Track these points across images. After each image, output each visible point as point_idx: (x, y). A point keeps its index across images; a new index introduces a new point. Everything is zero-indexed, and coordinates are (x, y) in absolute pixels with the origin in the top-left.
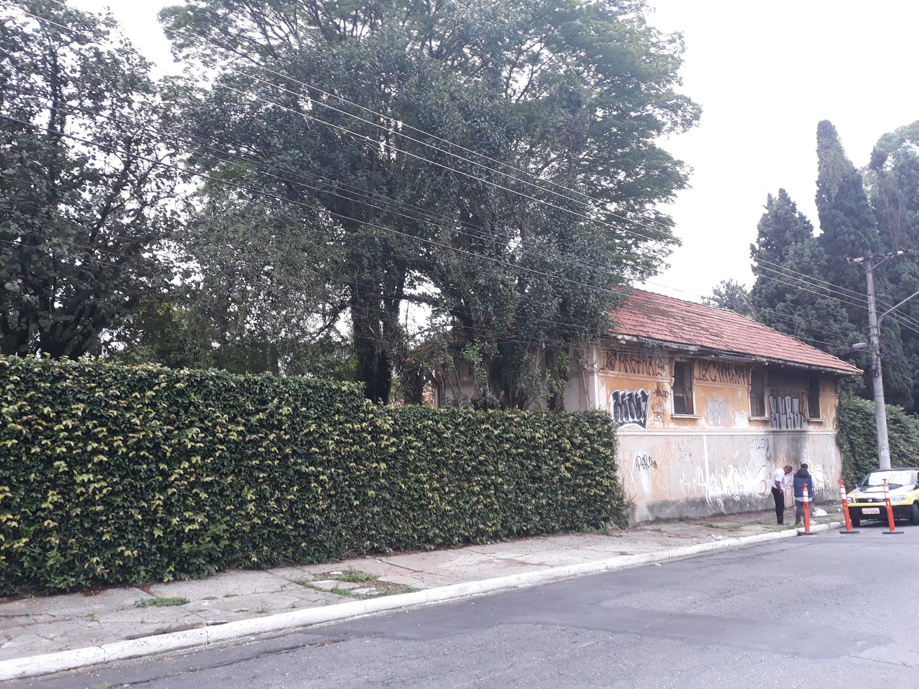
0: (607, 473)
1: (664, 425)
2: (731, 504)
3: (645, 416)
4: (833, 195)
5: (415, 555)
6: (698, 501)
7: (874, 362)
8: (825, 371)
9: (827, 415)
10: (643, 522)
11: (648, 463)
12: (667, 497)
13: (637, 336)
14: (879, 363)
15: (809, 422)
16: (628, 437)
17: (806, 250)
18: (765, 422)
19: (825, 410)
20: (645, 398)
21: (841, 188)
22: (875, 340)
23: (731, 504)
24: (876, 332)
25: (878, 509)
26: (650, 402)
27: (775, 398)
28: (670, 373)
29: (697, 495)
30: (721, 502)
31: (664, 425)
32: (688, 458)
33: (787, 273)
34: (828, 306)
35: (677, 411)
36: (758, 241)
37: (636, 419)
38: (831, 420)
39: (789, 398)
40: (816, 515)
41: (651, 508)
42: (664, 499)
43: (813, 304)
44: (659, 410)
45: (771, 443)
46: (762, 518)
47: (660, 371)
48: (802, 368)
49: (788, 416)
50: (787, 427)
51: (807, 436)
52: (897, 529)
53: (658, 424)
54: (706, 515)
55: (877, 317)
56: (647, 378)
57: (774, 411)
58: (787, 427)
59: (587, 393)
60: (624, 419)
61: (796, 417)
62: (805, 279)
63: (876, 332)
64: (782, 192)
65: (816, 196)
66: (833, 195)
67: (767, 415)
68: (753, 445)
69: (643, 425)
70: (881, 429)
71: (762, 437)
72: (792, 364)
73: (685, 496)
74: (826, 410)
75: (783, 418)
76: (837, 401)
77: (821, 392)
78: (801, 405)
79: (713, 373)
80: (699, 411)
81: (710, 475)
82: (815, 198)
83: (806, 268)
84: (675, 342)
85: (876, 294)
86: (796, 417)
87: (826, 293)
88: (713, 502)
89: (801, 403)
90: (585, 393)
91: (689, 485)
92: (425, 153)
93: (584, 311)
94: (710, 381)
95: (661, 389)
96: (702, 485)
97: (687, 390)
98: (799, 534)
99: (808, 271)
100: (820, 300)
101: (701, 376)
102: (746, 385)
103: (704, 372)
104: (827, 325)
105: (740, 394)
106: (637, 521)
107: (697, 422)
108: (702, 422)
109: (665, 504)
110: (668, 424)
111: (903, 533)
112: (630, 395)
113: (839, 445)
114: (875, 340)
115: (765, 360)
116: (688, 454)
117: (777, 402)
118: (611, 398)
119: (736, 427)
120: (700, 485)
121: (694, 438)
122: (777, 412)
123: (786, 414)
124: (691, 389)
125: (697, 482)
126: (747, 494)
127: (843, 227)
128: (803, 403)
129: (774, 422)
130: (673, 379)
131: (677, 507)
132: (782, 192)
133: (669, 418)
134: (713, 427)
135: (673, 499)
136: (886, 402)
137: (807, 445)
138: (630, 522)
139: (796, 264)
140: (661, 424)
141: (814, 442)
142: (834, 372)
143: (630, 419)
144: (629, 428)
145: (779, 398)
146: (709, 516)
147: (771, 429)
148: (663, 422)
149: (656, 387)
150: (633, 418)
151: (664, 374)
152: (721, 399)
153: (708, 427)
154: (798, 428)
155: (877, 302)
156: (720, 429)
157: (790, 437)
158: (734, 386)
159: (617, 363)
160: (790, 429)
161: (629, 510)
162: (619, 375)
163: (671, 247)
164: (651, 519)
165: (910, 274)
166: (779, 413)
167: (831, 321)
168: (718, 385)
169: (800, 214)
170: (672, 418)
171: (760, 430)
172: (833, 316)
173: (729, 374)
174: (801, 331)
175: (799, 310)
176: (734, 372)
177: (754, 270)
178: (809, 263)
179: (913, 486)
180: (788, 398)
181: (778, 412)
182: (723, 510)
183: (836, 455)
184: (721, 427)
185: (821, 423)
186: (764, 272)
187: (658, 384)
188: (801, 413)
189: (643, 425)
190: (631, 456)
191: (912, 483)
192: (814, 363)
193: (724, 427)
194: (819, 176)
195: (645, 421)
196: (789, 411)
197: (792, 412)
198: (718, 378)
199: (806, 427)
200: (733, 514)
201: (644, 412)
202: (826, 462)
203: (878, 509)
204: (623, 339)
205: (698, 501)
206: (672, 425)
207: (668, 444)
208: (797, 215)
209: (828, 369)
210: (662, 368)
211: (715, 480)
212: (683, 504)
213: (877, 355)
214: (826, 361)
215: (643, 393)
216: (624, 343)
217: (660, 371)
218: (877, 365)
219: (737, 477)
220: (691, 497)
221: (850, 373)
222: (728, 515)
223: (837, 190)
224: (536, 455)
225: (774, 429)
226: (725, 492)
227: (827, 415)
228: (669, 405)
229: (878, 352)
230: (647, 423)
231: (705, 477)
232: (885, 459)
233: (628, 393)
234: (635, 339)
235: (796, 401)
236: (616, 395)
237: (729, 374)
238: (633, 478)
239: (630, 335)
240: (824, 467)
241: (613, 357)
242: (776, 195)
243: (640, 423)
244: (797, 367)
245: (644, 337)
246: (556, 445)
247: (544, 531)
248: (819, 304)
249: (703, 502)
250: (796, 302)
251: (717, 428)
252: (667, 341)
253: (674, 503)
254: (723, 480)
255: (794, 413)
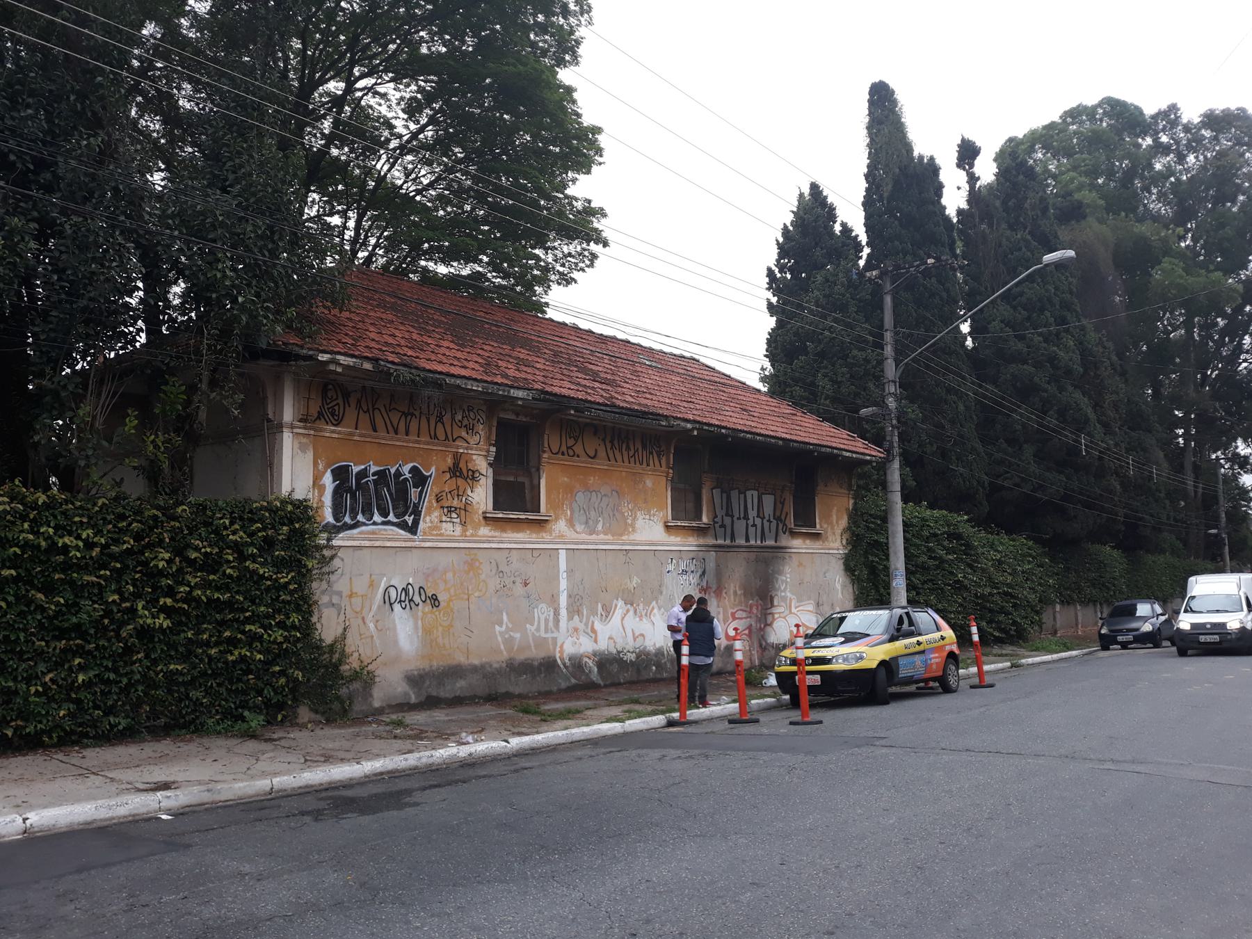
0: (279, 618)
1: (464, 531)
2: (615, 668)
3: (417, 513)
4: (886, 195)
5: (23, 758)
6: (536, 663)
7: (888, 438)
8: (819, 453)
9: (830, 523)
10: (390, 706)
11: (417, 599)
12: (461, 659)
13: (375, 360)
14: (896, 439)
15: (793, 534)
16: (365, 551)
17: (841, 275)
18: (701, 531)
19: (827, 517)
20: (420, 479)
21: (897, 183)
22: (892, 403)
23: (615, 668)
24: (892, 390)
25: (818, 677)
26: (431, 489)
27: (726, 492)
28: (488, 438)
29: (535, 654)
30: (590, 663)
31: (464, 531)
32: (519, 590)
33: (811, 312)
34: (867, 361)
35: (497, 506)
36: (778, 264)
37: (391, 517)
38: (838, 531)
39: (755, 493)
40: (768, 684)
41: (415, 680)
42: (455, 663)
43: (845, 357)
44: (455, 503)
45: (711, 565)
46: (654, 692)
47: (464, 434)
48: (770, 443)
49: (750, 522)
50: (747, 540)
51: (787, 556)
52: (814, 715)
53: (451, 529)
54: (555, 689)
55: (897, 366)
56: (428, 444)
57: (720, 513)
58: (747, 540)
59: (271, 465)
60: (360, 518)
61: (766, 524)
62: (836, 320)
63: (892, 390)
64: (814, 187)
65: (864, 197)
66: (886, 195)
67: (705, 519)
68: (670, 567)
69: (413, 529)
70: (894, 543)
71: (692, 555)
72: (848, 454)
73: (505, 655)
74: (830, 516)
75: (740, 526)
76: (852, 501)
77: (820, 487)
78: (779, 506)
79: (592, 444)
80: (552, 504)
81: (570, 618)
82: (862, 199)
83: (838, 303)
84: (475, 380)
85: (895, 328)
86: (766, 524)
87: (866, 341)
88: (573, 665)
89: (779, 504)
90: (270, 465)
91: (518, 635)
92: (109, 33)
93: (209, 295)
94: (584, 458)
95: (462, 465)
96: (549, 635)
97: (533, 470)
98: (671, 723)
99: (843, 308)
100: (855, 352)
101: (564, 448)
102: (664, 468)
103: (571, 442)
104: (865, 390)
105: (649, 483)
106: (377, 704)
107: (548, 526)
108: (561, 526)
109: (456, 672)
110: (476, 528)
111: (821, 722)
112: (382, 475)
113: (849, 569)
114: (892, 403)
115: (689, 426)
116: (518, 580)
117: (729, 498)
118: (328, 479)
119: (637, 537)
120: (543, 635)
121: (536, 554)
122: (727, 515)
123: (746, 518)
124: (538, 470)
125: (538, 629)
126: (651, 649)
127: (897, 243)
128: (783, 504)
129: (720, 531)
130: (493, 449)
131: (485, 676)
132: (814, 187)
133: (478, 517)
134: (584, 537)
135: (476, 662)
136: (905, 500)
137: (787, 569)
138: (358, 707)
139: (825, 296)
140: (459, 529)
141: (800, 564)
142: (838, 456)
143: (377, 518)
144: (373, 533)
145: (734, 494)
146: (560, 691)
147: (712, 541)
148: (463, 524)
149: (450, 461)
150: (384, 514)
151: (473, 440)
152: (605, 490)
153: (574, 535)
154: (770, 542)
155: (896, 341)
156: (602, 540)
157: (752, 556)
158: (638, 468)
159: (351, 414)
160: (752, 542)
161: (356, 685)
162: (351, 434)
163: (593, 247)
164: (413, 699)
165: (1002, 322)
166: (732, 516)
167: (871, 385)
168: (601, 464)
169: (844, 225)
170: (485, 518)
171: (689, 543)
172: (874, 376)
173: (628, 449)
174: (825, 399)
175: (826, 368)
176: (639, 446)
177: (771, 308)
178: (844, 295)
179: (885, 637)
180: (752, 495)
181: (729, 513)
182: (595, 675)
183: (844, 587)
184: (602, 536)
185: (817, 536)
186: (783, 311)
187: (457, 457)
188: (778, 519)
189: (413, 529)
190: (372, 585)
191: (886, 631)
192: (794, 438)
193: (610, 537)
194: (868, 167)
195: (416, 523)
196: (752, 513)
197: (760, 515)
198: (602, 453)
199: (785, 541)
200: (617, 685)
201: (416, 506)
202: (824, 598)
203: (818, 677)
204: (333, 361)
205: (536, 663)
206: (485, 531)
207: (472, 566)
208: (837, 228)
209: (823, 450)
210: (470, 429)
211: (581, 626)
212: (499, 671)
213: (892, 426)
214: (828, 438)
215: (414, 470)
216: (339, 370)
217: (464, 434)
218: (891, 442)
219: (630, 620)
220: (521, 657)
221: (868, 458)
222: (606, 686)
223: (890, 187)
224: (72, 583)
225: (720, 542)
226: (603, 645)
227: (830, 523)
228: (481, 496)
229: (894, 422)
230: (421, 526)
231: (557, 621)
232: (898, 593)
233: (374, 469)
234: (368, 366)
235: (768, 501)
236: (341, 474)
237: (628, 449)
238: (372, 626)
239: (353, 356)
240: (818, 604)
241: (340, 401)
242: (806, 191)
243: (403, 526)
244: (759, 442)
245: (393, 363)
246: (140, 563)
247: (127, 735)
248: (854, 357)
249: (549, 665)
250: (822, 355)
251: (594, 536)
252: (453, 376)
253: (475, 669)
254: (597, 626)
255: (763, 519)
